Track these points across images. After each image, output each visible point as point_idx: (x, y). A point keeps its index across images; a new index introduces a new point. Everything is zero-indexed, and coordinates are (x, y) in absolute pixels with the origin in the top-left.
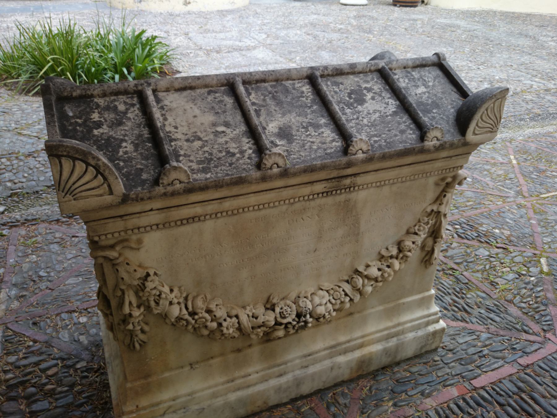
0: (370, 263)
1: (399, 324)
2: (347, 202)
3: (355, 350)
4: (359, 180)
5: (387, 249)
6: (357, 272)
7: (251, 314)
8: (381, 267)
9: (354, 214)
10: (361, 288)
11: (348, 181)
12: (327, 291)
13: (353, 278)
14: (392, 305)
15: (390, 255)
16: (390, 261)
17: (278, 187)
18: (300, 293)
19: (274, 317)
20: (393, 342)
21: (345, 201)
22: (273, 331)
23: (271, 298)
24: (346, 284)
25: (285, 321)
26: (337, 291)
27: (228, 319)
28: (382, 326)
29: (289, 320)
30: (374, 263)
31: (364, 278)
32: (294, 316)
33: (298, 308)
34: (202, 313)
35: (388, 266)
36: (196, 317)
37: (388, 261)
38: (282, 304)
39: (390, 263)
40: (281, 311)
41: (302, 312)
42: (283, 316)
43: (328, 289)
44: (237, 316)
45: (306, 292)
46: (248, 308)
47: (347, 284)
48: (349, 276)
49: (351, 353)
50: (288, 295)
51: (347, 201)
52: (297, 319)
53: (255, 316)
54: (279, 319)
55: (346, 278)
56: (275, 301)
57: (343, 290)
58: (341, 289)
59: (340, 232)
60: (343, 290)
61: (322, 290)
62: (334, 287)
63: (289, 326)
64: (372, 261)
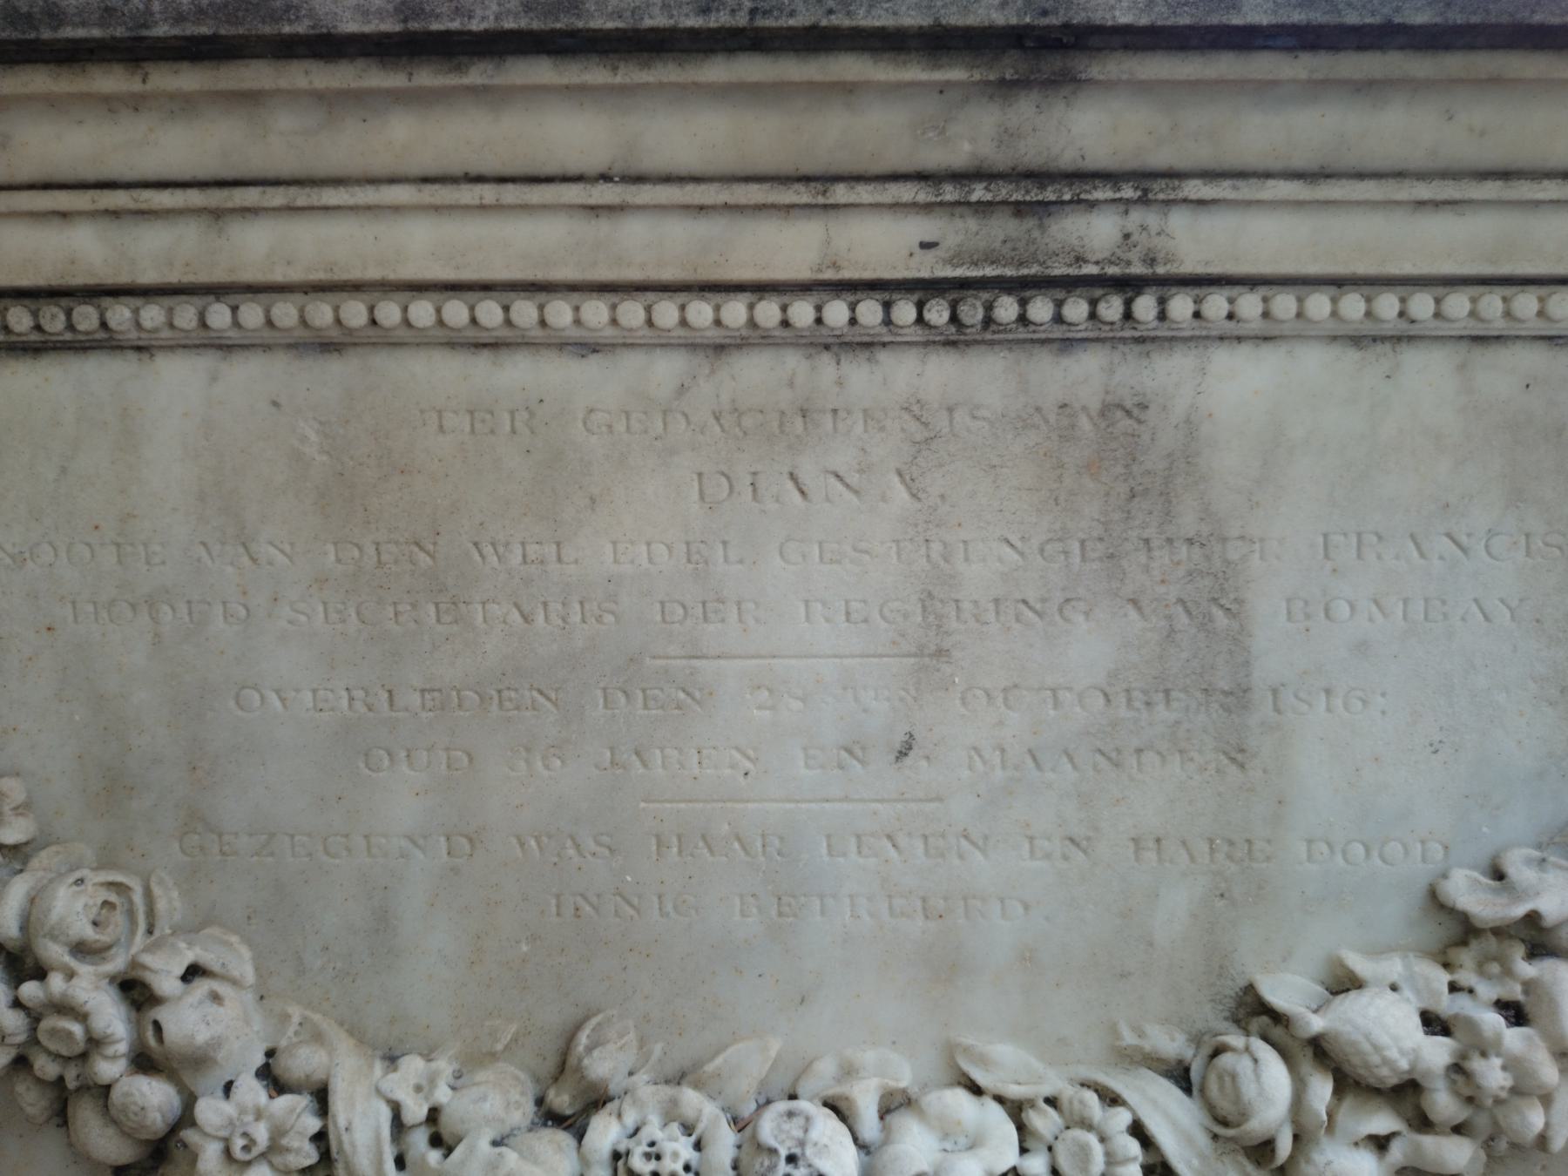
0: (1358, 963)
2: (1125, 423)
4: (1192, 239)
5: (1499, 875)
6: (1255, 1012)
7: (415, 1111)
8: (1447, 1005)
9: (1188, 520)
10: (1284, 1147)
11: (1096, 233)
12: (1016, 1110)
13: (1218, 1051)
15: (1520, 911)
16: (1527, 970)
17: (573, 168)
18: (806, 1069)
21: (1106, 410)
23: (583, 1039)
24: (1168, 1092)
26: (1087, 1125)
27: (252, 1091)
30: (1394, 967)
31: (1307, 1065)
34: (70, 975)
35: (1515, 1013)
36: (30, 990)
37: (1508, 972)
39: (1529, 986)
43: (1014, 1091)
44: (321, 1097)
45: (849, 1071)
46: (413, 1066)
47: (1178, 1093)
48: (1196, 1040)
51: (1126, 412)
53: (447, 1125)
55: (1172, 1045)
56: (603, 1066)
57: (1138, 1130)
58: (1122, 1118)
59: (1090, 648)
60: (1138, 1130)
61: (976, 1090)
62: (1067, 1091)
64: (1376, 951)
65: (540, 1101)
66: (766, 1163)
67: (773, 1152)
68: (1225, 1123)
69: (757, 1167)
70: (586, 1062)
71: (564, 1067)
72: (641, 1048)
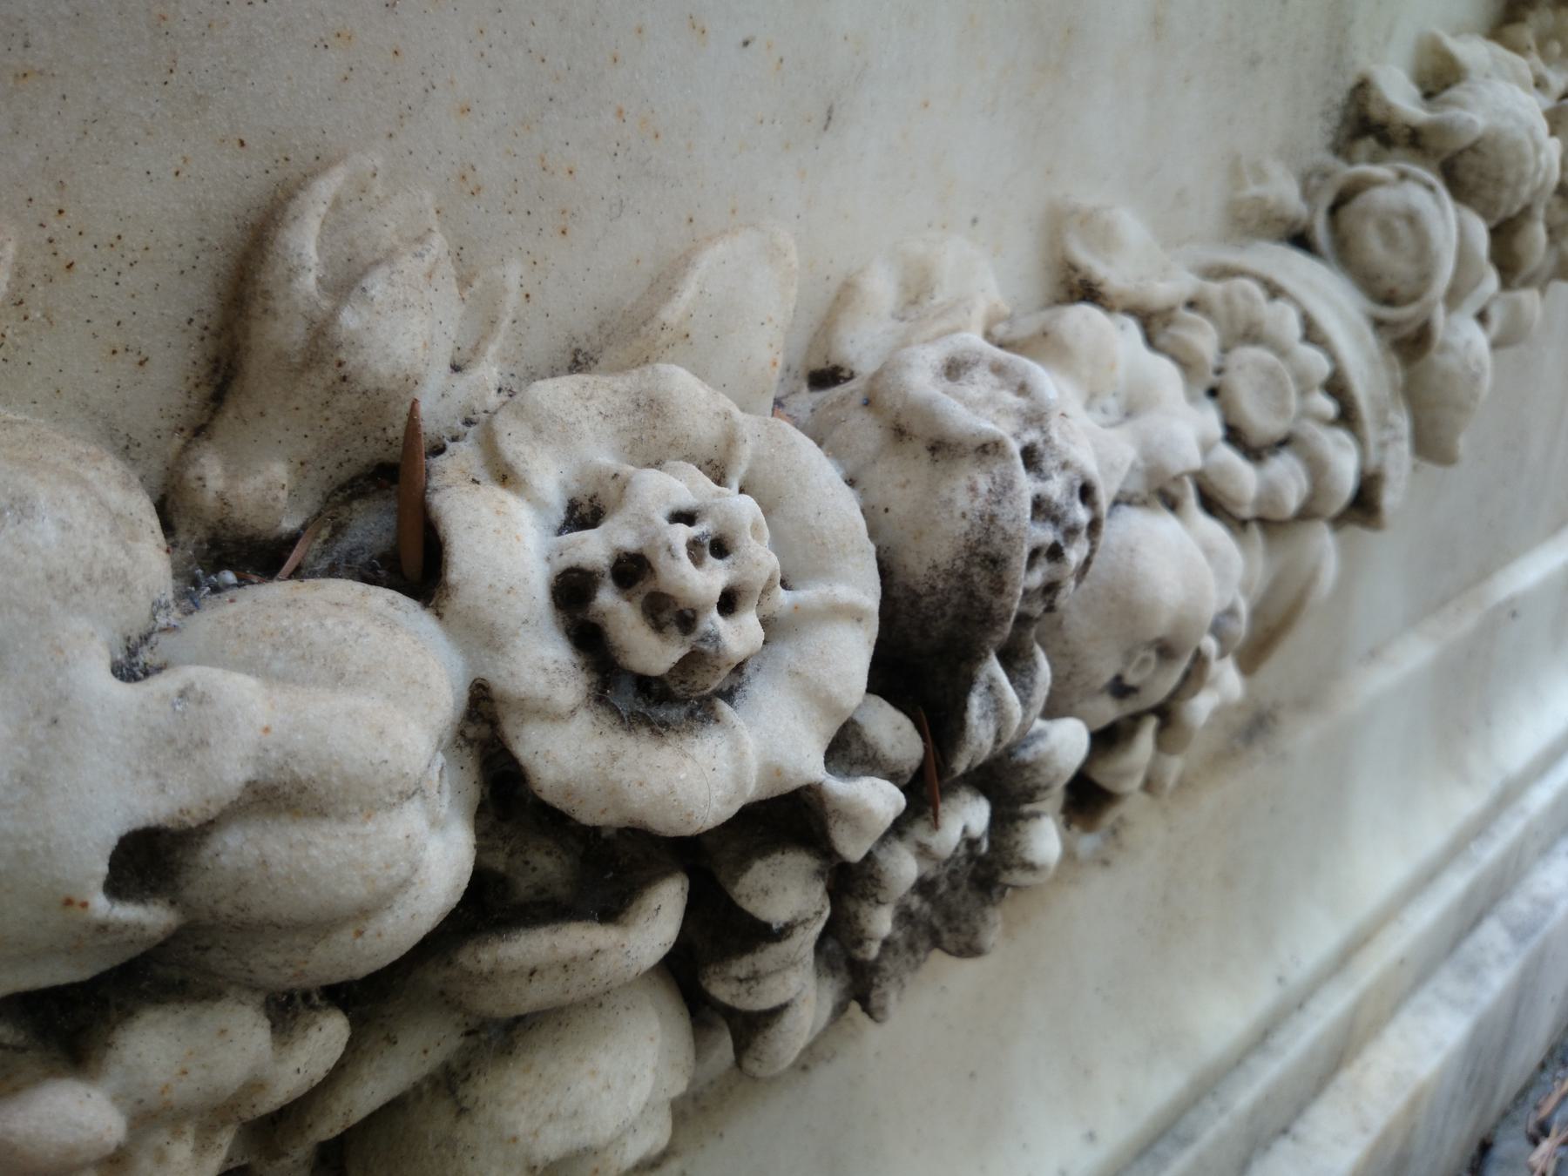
1: (1508, 796)
3: (1300, 1108)
6: (1363, 125)
14: (1467, 622)
19: (445, 698)
20: (1497, 962)
22: (449, 1083)
23: (306, 244)
25: (697, 778)
28: (1432, 836)
29: (764, 741)
32: (849, 655)
33: (904, 483)
38: (569, 435)
40: (594, 548)
41: (986, 558)
42: (654, 653)
49: (1284, 1146)
50: (665, 283)
52: (894, 733)
54: (572, 752)
63: (785, 891)
65: (168, 510)
66: (983, 483)
67: (989, 449)
68: (1389, 300)
69: (962, 501)
70: (350, 319)
71: (235, 346)
72: (464, 282)
